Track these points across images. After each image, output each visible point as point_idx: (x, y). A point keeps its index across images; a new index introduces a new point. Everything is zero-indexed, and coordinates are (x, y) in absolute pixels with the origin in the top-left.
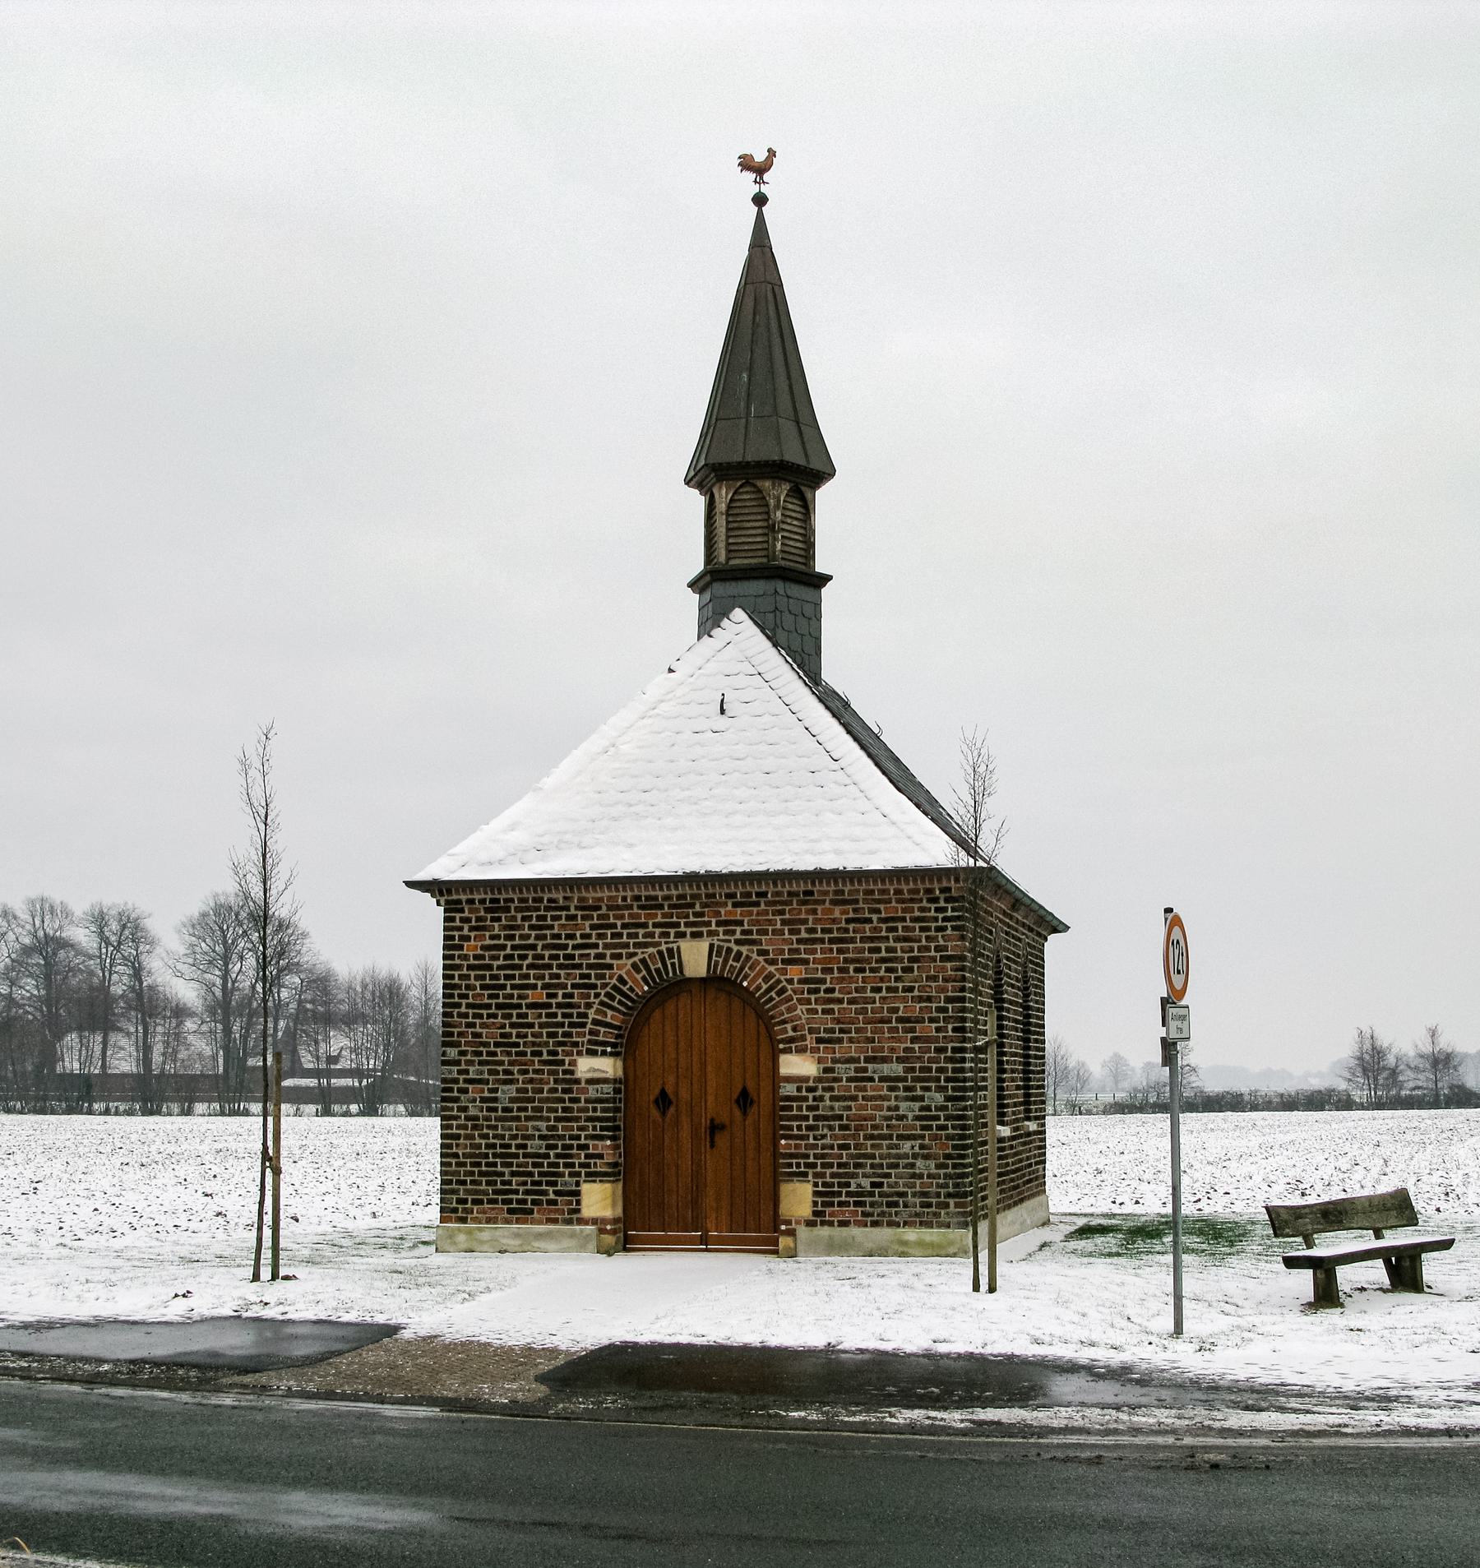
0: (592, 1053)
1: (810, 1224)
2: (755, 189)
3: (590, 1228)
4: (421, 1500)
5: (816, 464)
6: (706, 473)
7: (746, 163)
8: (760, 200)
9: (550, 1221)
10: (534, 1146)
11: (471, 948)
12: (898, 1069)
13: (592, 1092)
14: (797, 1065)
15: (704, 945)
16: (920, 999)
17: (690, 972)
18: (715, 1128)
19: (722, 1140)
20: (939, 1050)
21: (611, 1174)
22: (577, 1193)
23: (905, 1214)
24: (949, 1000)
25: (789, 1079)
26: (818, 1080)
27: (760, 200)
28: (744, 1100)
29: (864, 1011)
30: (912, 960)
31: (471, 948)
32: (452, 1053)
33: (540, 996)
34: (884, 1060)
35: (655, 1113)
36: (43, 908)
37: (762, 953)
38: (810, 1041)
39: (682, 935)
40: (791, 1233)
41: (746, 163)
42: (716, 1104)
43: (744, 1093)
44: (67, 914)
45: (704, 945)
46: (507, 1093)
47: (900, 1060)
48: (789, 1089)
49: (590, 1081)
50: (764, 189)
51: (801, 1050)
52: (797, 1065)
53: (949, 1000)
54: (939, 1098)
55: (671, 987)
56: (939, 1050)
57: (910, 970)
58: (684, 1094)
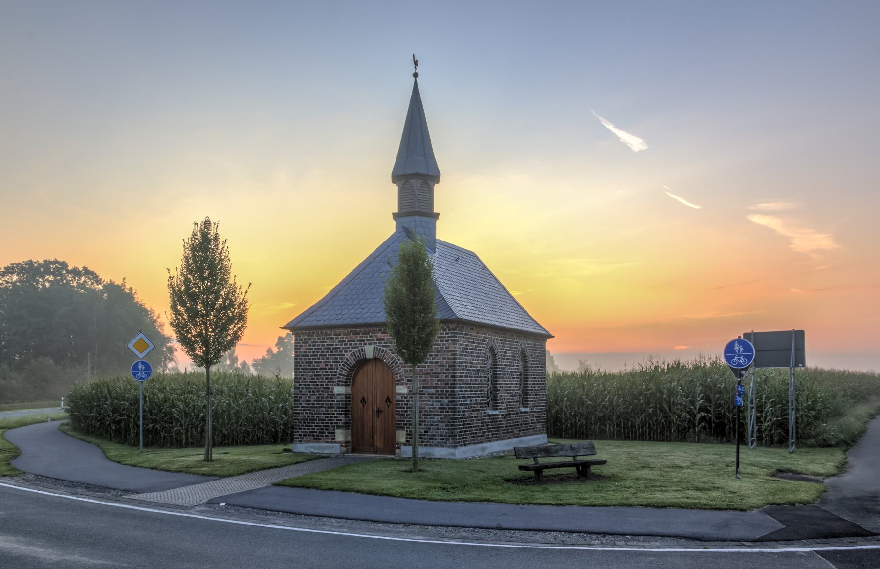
0: (338, 385)
1: (405, 445)
3: (338, 445)
4: (89, 438)
5: (431, 173)
6: (398, 177)
8: (416, 75)
9: (327, 442)
10: (322, 416)
11: (303, 349)
12: (433, 391)
13: (339, 398)
14: (402, 389)
15: (372, 347)
16: (440, 366)
17: (368, 357)
18: (379, 411)
19: (381, 415)
20: (447, 384)
21: (346, 426)
22: (334, 433)
23: (435, 442)
24: (450, 366)
25: (399, 394)
26: (408, 394)
27: (416, 75)
28: (388, 400)
29: (422, 370)
30: (438, 352)
31: (303, 349)
32: (297, 385)
33: (322, 365)
34: (429, 387)
35: (361, 405)
37: (390, 350)
38: (405, 381)
39: (365, 344)
40: (399, 448)
42: (380, 403)
43: (388, 398)
45: (372, 347)
46: (313, 398)
47: (434, 387)
48: (399, 397)
49: (338, 395)
51: (402, 384)
52: (402, 389)
53: (450, 366)
54: (446, 401)
55: (362, 362)
56: (447, 384)
57: (436, 355)
58: (370, 399)
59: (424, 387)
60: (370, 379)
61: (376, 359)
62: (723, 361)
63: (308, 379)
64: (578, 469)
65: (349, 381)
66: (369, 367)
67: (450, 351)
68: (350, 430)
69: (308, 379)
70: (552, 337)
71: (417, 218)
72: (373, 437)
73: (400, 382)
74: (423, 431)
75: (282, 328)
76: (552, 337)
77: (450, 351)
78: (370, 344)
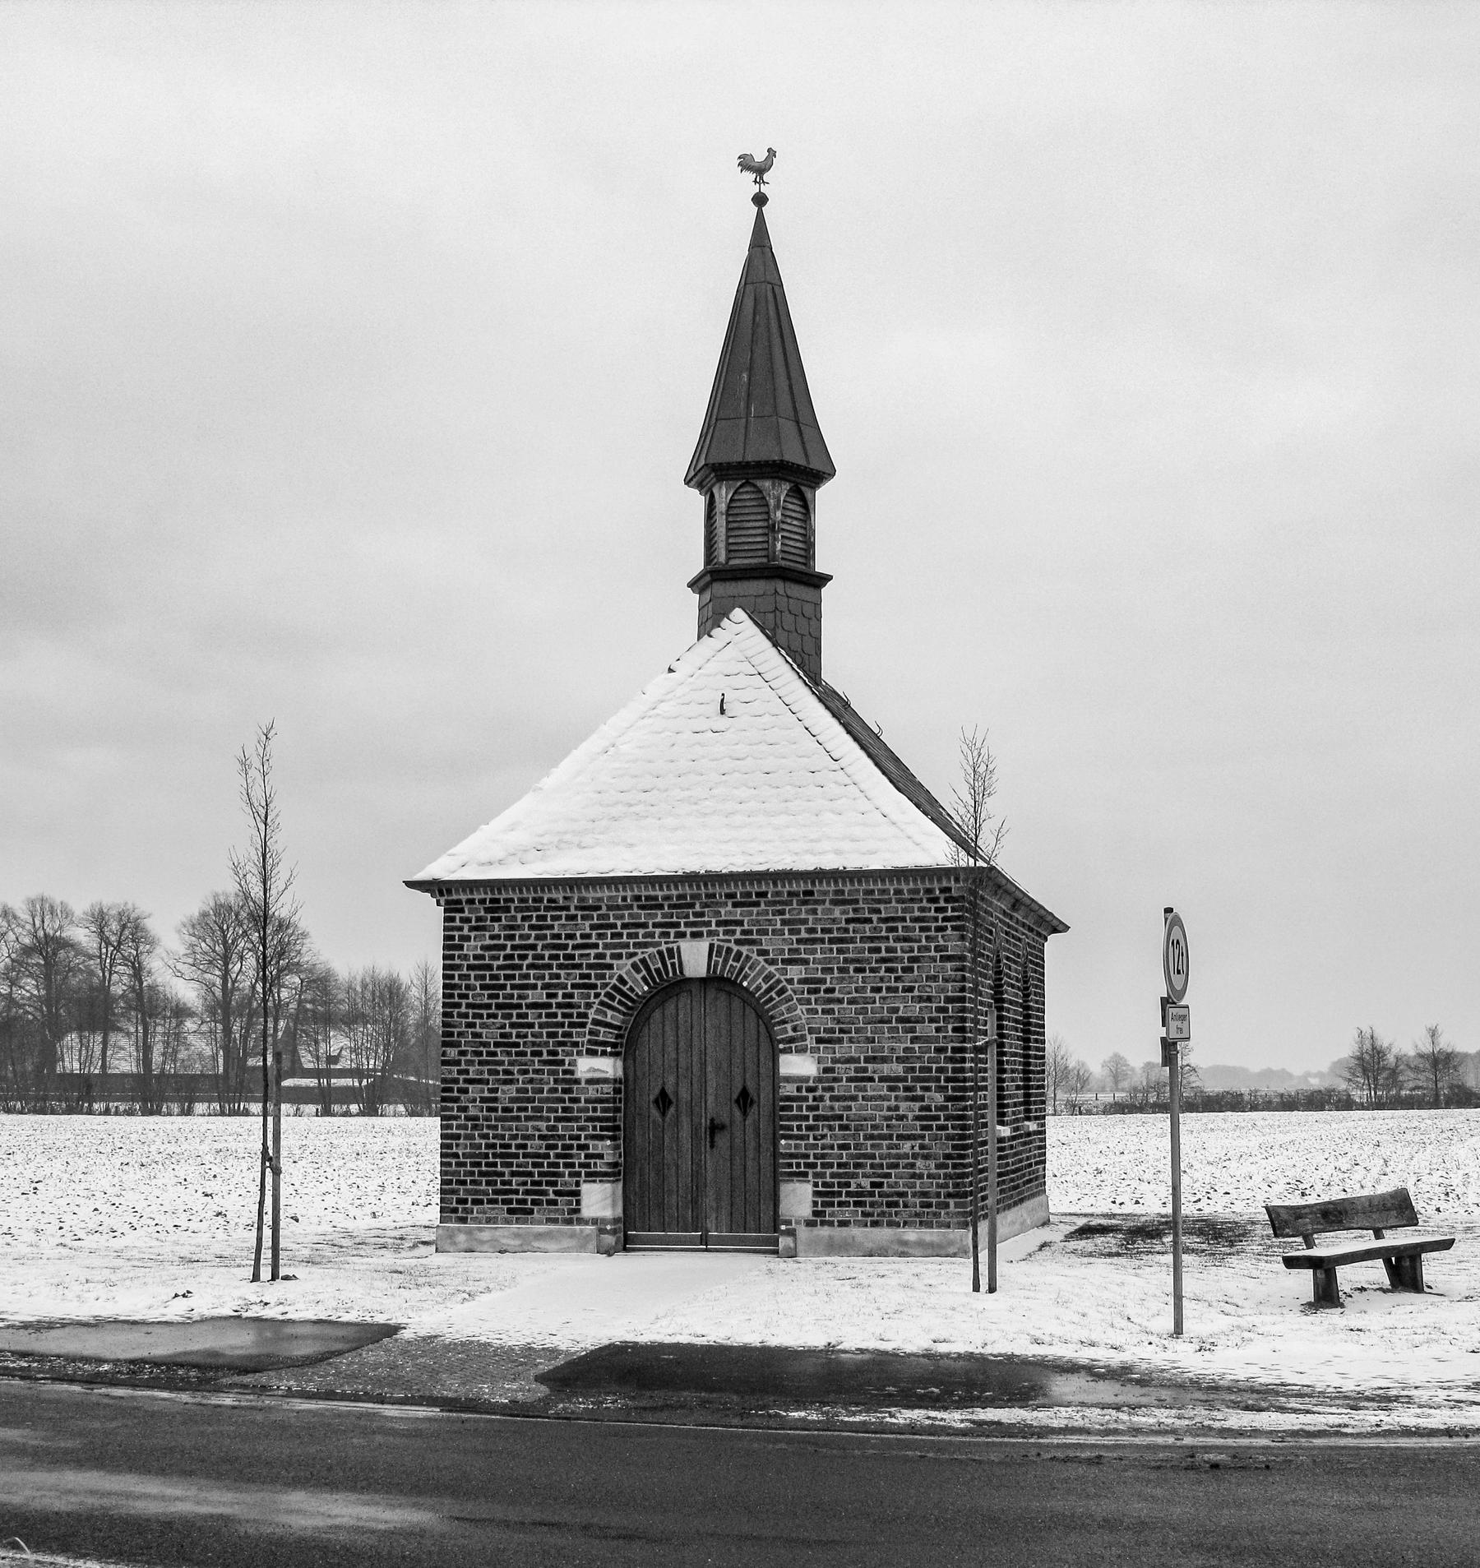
0: (592, 1053)
1: (810, 1224)
2: (756, 189)
5: (816, 464)
6: (707, 473)
7: (746, 163)
8: (760, 200)
10: (534, 1145)
11: (472, 948)
12: (898, 1069)
13: (592, 1091)
15: (703, 946)
16: (920, 999)
17: (689, 972)
18: (715, 1128)
19: (722, 1140)
21: (612, 1174)
22: (577, 1193)
25: (788, 1079)
26: (819, 1080)
27: (760, 200)
28: (744, 1100)
30: (913, 960)
31: (472, 948)
32: (452, 1053)
33: (538, 995)
34: (884, 1060)
36: (43, 907)
38: (810, 1041)
39: (682, 935)
41: (746, 163)
42: (716, 1104)
44: (67, 913)
45: (703, 946)
46: (507, 1093)
48: (789, 1089)
49: (590, 1081)
50: (764, 189)
51: (801, 1051)
52: (798, 1065)
53: (949, 1000)
54: (939, 1098)
55: (670, 986)
57: (910, 970)
58: (684, 1094)
59: (873, 1060)
60: (699, 1040)
61: (714, 982)
62: (1139, 1071)
63: (490, 1035)
64: (1388, 1262)
65: (625, 1046)
66: (682, 1007)
67: (949, 958)
68: (620, 1185)
69: (490, 1035)
70: (1058, 927)
71: (780, 586)
72: (695, 1203)
73: (794, 1044)
74: (866, 1183)
75: (411, 884)
76: (1058, 927)
77: (949, 958)
78: (695, 935)
